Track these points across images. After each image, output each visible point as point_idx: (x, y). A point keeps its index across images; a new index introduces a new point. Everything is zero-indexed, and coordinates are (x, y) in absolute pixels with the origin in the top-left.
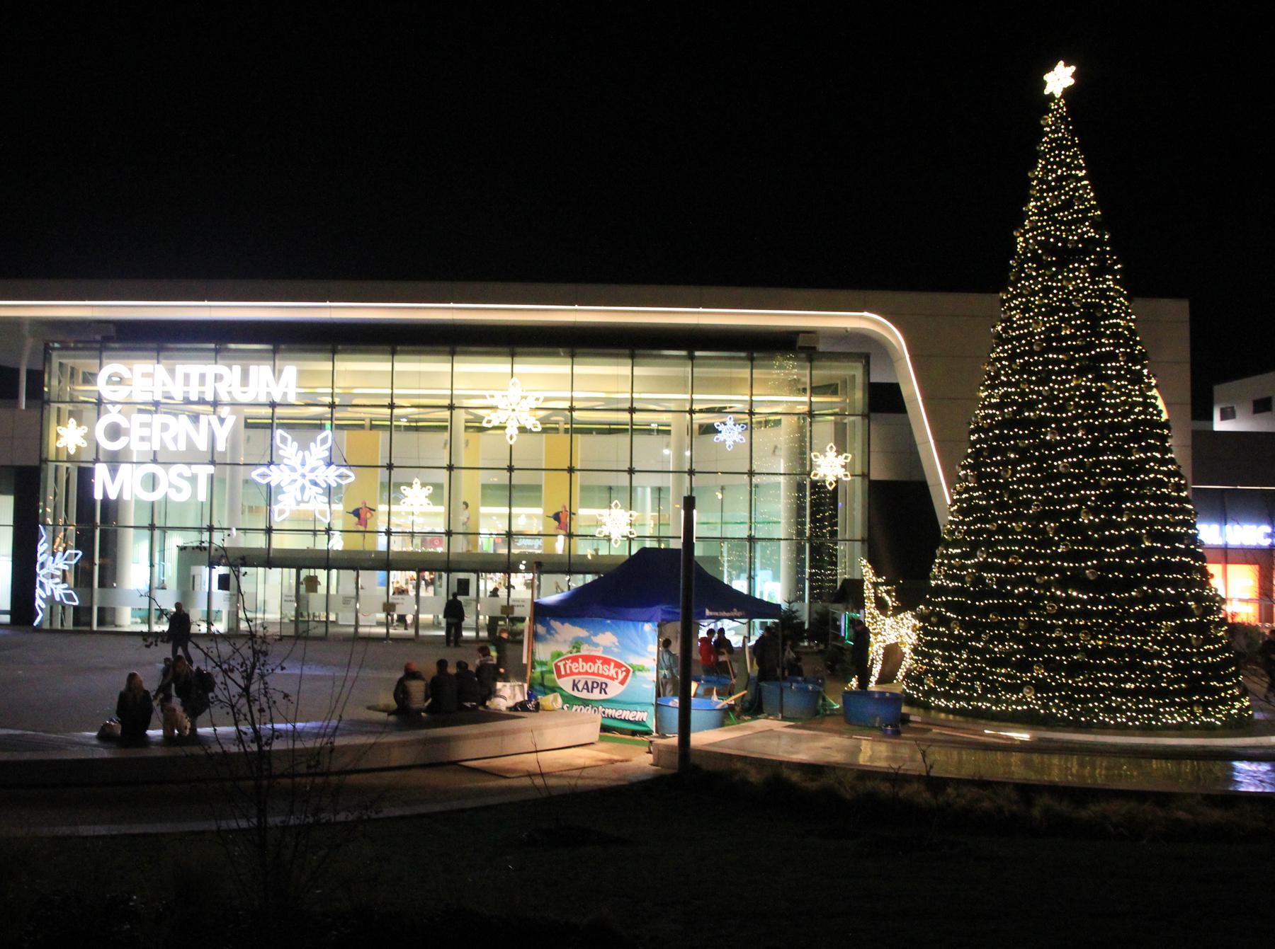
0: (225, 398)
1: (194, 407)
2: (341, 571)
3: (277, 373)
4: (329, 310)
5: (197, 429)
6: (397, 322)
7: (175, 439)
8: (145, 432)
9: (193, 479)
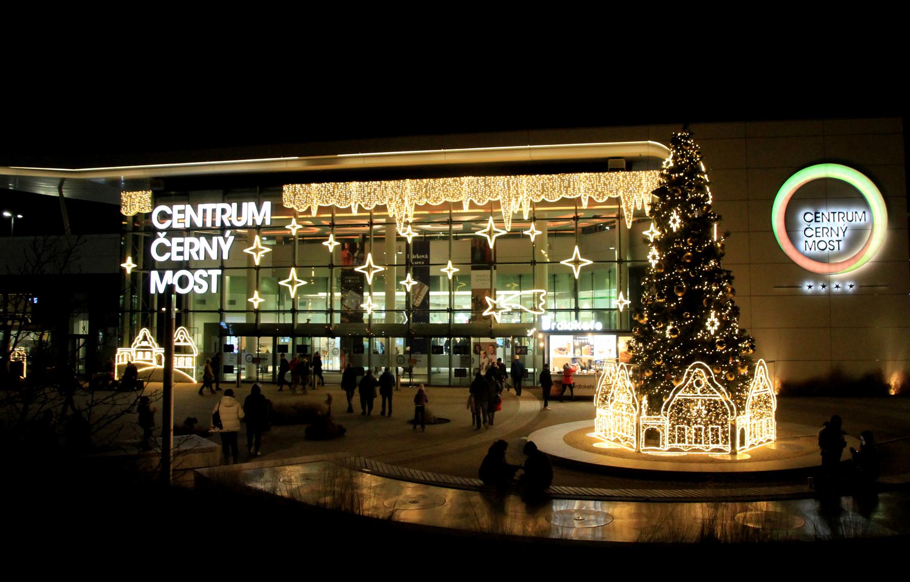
0: (228, 224)
1: (207, 233)
3: (259, 209)
4: (529, 151)
7: (198, 253)
8: (180, 249)
9: (208, 279)
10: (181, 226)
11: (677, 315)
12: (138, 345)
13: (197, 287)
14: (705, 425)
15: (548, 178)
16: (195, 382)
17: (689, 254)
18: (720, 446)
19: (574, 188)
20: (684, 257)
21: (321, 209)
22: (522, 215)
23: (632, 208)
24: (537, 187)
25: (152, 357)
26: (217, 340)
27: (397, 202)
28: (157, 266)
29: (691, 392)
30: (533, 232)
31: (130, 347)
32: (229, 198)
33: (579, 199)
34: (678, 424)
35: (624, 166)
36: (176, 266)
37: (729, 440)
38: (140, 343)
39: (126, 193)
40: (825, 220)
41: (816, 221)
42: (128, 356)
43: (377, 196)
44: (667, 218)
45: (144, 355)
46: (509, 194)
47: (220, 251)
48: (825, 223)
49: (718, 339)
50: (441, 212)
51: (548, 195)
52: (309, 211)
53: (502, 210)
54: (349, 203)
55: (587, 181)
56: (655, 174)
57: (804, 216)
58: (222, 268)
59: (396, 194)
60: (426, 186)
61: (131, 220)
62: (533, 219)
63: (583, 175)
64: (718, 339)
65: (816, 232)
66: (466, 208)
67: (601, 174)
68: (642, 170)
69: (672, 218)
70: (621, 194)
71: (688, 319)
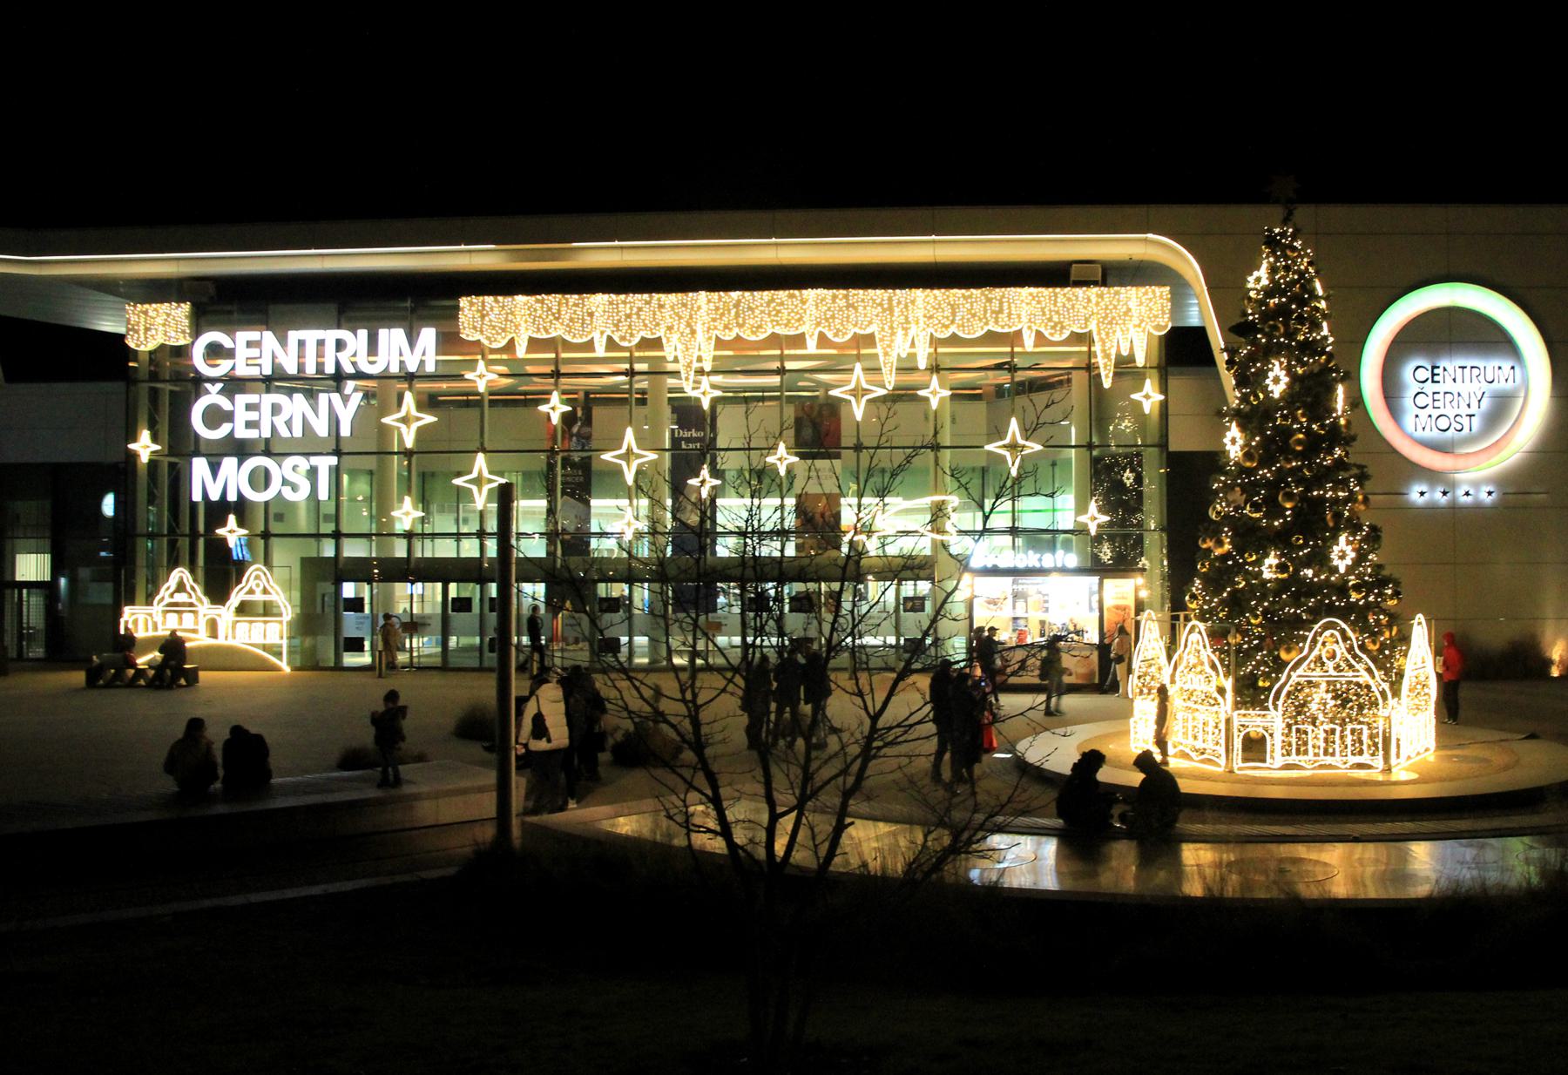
0: (349, 369)
1: (307, 385)
2: (461, 584)
3: (412, 339)
5: (315, 411)
6: (608, 269)
7: (289, 423)
8: (253, 416)
10: (254, 372)
11: (1281, 539)
12: (168, 600)
13: (289, 488)
14: (1341, 725)
15: (963, 294)
16: (287, 669)
17: (1301, 436)
18: (1365, 758)
19: (1010, 314)
20: (1291, 441)
21: (534, 344)
22: (916, 361)
23: (1113, 352)
24: (943, 311)
25: (196, 623)
26: (331, 588)
27: (682, 334)
28: (203, 448)
29: (1318, 669)
30: (936, 393)
31: (151, 604)
32: (350, 320)
33: (1019, 333)
34: (1296, 723)
35: (1099, 278)
36: (241, 450)
37: (1380, 749)
38: (172, 595)
39: (135, 306)
40: (1449, 380)
41: (1433, 382)
42: (147, 620)
43: (644, 320)
44: (1263, 374)
45: (181, 618)
46: (892, 322)
47: (335, 422)
48: (1448, 385)
49: (1352, 580)
50: (756, 353)
51: (963, 326)
52: (510, 346)
53: (879, 350)
54: (590, 332)
55: (1034, 303)
56: (1154, 292)
57: (1412, 372)
58: (337, 452)
59: (680, 318)
60: (737, 305)
61: (147, 358)
62: (935, 368)
63: (1026, 292)
64: (1352, 580)
65: (1434, 400)
66: (812, 347)
67: (1058, 290)
68: (1133, 286)
69: (1271, 375)
70: (1092, 326)
71: (1301, 548)
